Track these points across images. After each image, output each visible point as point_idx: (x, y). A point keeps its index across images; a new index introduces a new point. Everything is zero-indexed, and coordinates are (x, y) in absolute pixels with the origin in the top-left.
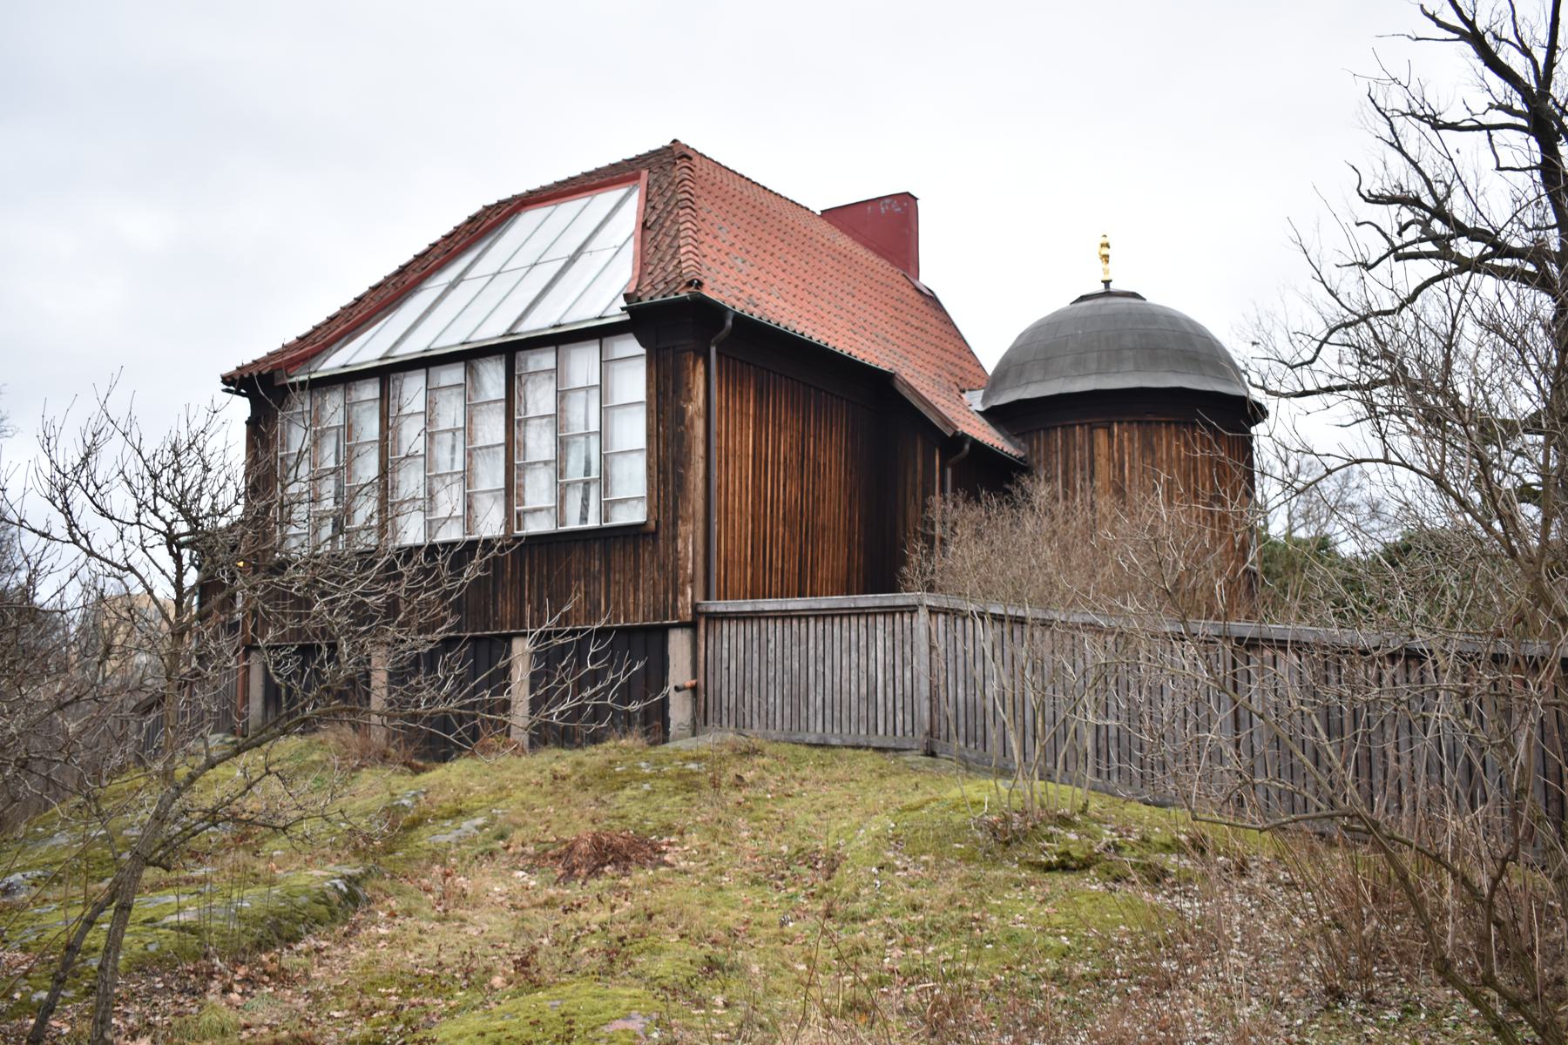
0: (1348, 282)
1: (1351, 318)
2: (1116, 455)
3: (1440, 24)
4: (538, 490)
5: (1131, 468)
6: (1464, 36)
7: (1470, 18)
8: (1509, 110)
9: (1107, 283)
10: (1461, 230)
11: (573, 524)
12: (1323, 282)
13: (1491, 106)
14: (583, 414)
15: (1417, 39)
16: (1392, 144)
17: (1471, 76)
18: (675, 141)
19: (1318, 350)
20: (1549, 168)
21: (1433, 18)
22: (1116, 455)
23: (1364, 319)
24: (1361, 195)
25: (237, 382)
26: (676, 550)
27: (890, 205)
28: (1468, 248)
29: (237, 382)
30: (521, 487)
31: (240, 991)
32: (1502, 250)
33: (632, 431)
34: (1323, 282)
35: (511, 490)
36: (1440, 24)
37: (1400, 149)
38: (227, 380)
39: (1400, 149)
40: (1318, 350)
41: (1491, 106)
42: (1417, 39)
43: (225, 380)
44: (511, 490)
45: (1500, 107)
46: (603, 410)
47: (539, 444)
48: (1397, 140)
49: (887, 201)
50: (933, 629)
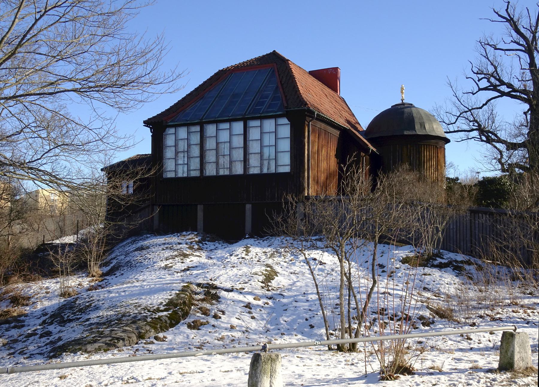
0: (464, 98)
1: (467, 110)
2: (409, 154)
3: (500, 16)
4: (254, 161)
5: (413, 157)
6: (508, 21)
7: (512, 17)
8: (518, 44)
9: (402, 100)
10: (502, 83)
11: (265, 171)
12: (456, 97)
13: (512, 41)
14: (269, 140)
15: (493, 21)
16: (485, 57)
17: (506, 31)
18: (274, 51)
19: (457, 119)
20: (532, 64)
21: (497, 13)
22: (409, 154)
23: (470, 110)
24: (473, 71)
25: (147, 123)
26: (300, 180)
27: (332, 71)
28: (504, 88)
29: (147, 123)
30: (249, 160)
31: (359, 295)
32: (515, 90)
33: (285, 145)
34: (456, 97)
35: (246, 161)
36: (500, 16)
37: (488, 58)
38: (144, 122)
39: (488, 58)
40: (457, 119)
41: (512, 41)
42: (493, 21)
43: (144, 122)
44: (246, 161)
45: (515, 42)
46: (276, 139)
47: (254, 147)
48: (487, 55)
49: (331, 70)
50: (473, 221)
